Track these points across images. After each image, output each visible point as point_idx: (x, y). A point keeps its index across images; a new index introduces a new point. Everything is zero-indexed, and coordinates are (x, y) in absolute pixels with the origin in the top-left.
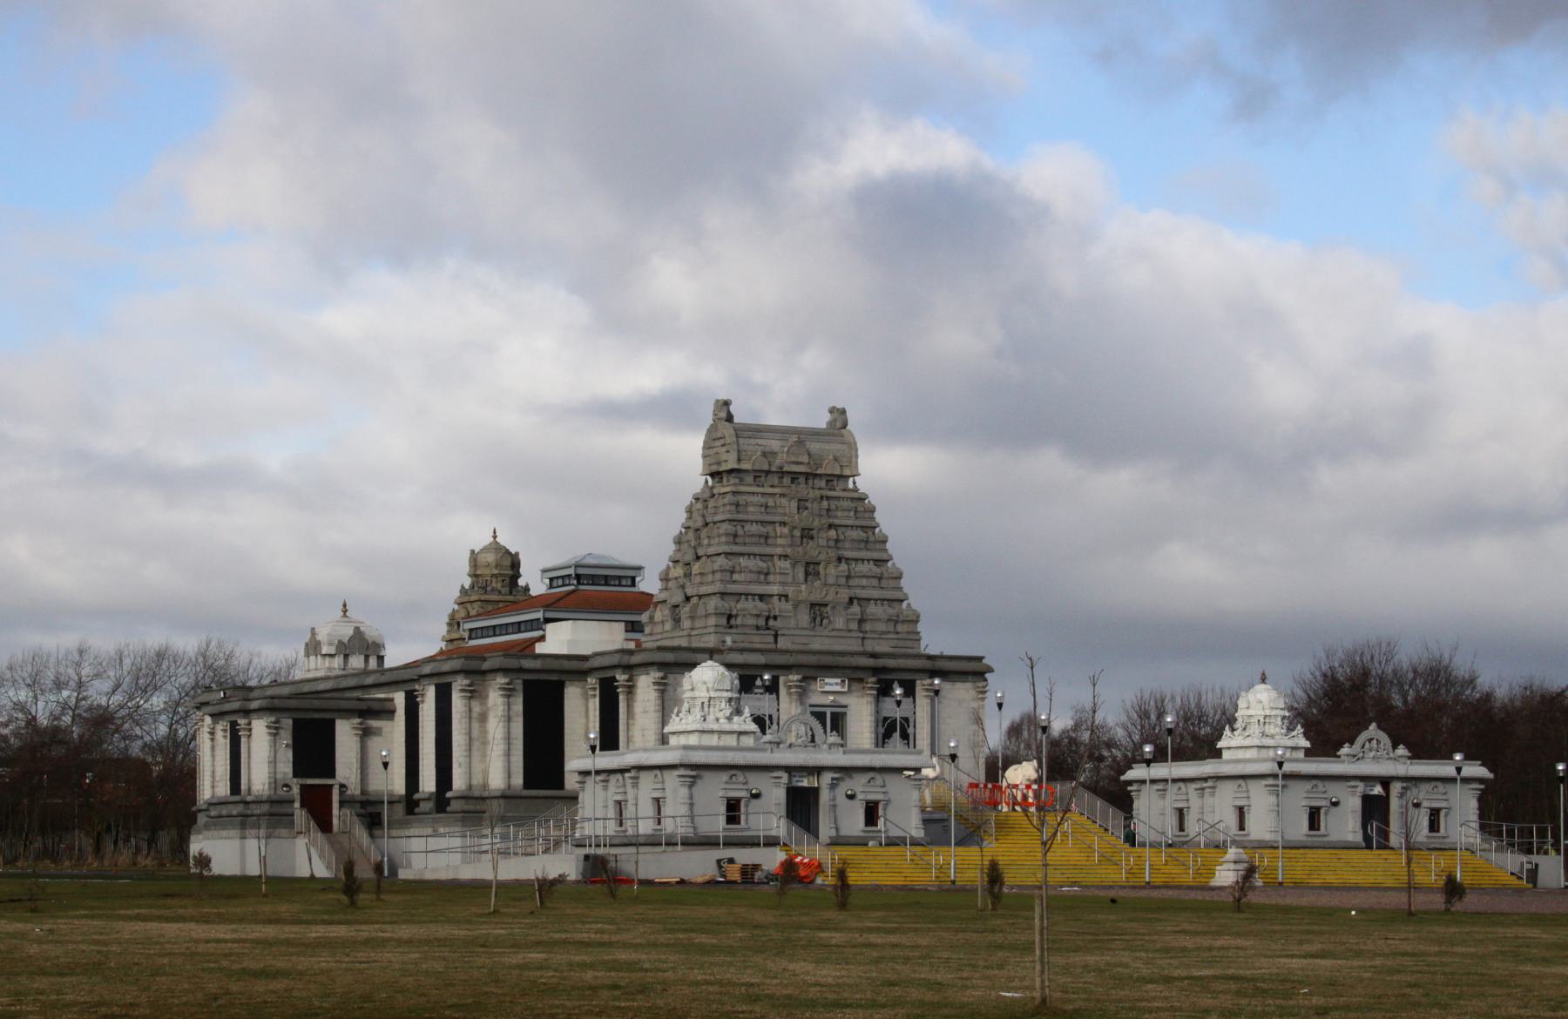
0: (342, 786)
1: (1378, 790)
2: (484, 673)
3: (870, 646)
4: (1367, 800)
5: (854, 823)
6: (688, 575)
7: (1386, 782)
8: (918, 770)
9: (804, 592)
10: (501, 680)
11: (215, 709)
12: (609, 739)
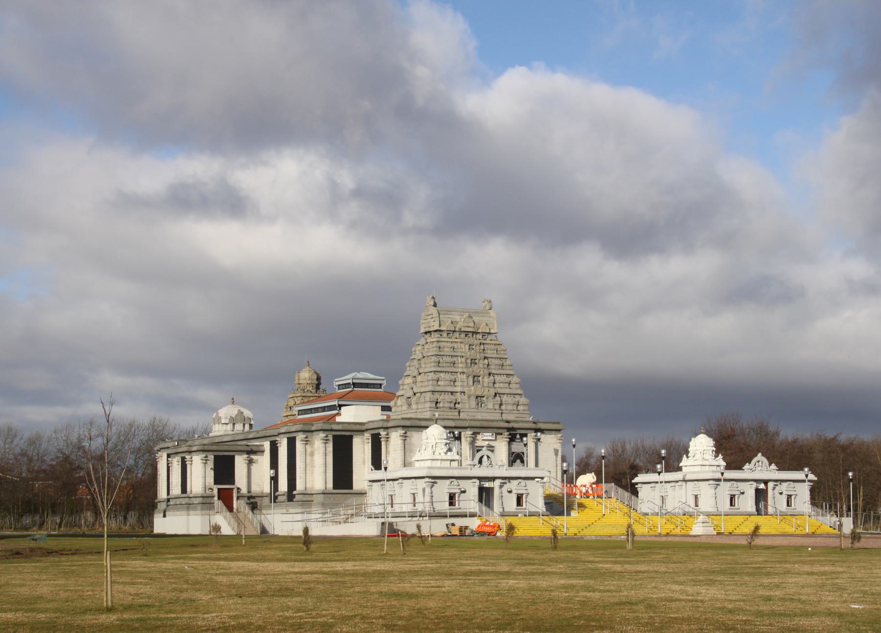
0: (238, 489)
1: (762, 486)
2: (312, 431)
3: (505, 417)
4: (757, 491)
5: (511, 504)
6: (415, 382)
7: (766, 482)
8: (542, 478)
9: (473, 390)
10: (322, 435)
11: (170, 451)
12: (377, 463)
